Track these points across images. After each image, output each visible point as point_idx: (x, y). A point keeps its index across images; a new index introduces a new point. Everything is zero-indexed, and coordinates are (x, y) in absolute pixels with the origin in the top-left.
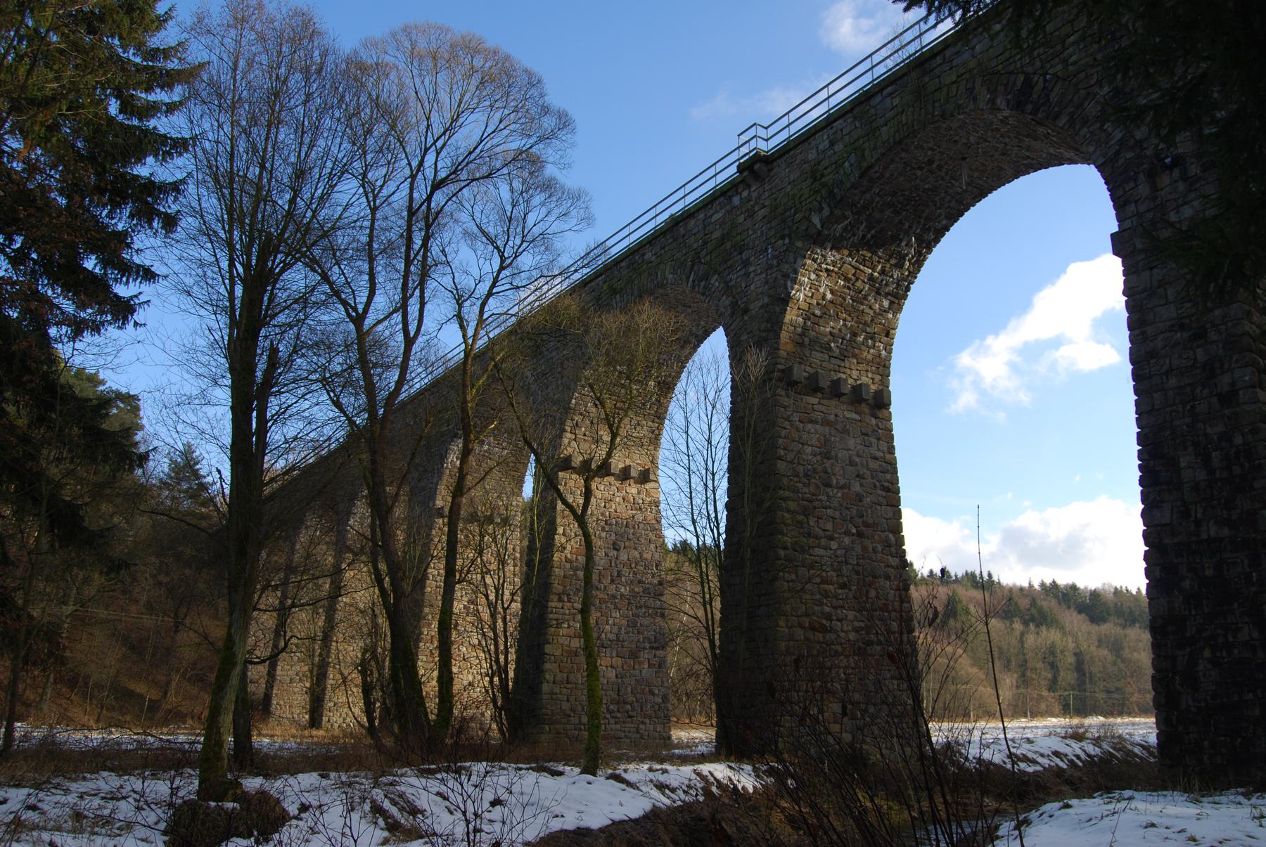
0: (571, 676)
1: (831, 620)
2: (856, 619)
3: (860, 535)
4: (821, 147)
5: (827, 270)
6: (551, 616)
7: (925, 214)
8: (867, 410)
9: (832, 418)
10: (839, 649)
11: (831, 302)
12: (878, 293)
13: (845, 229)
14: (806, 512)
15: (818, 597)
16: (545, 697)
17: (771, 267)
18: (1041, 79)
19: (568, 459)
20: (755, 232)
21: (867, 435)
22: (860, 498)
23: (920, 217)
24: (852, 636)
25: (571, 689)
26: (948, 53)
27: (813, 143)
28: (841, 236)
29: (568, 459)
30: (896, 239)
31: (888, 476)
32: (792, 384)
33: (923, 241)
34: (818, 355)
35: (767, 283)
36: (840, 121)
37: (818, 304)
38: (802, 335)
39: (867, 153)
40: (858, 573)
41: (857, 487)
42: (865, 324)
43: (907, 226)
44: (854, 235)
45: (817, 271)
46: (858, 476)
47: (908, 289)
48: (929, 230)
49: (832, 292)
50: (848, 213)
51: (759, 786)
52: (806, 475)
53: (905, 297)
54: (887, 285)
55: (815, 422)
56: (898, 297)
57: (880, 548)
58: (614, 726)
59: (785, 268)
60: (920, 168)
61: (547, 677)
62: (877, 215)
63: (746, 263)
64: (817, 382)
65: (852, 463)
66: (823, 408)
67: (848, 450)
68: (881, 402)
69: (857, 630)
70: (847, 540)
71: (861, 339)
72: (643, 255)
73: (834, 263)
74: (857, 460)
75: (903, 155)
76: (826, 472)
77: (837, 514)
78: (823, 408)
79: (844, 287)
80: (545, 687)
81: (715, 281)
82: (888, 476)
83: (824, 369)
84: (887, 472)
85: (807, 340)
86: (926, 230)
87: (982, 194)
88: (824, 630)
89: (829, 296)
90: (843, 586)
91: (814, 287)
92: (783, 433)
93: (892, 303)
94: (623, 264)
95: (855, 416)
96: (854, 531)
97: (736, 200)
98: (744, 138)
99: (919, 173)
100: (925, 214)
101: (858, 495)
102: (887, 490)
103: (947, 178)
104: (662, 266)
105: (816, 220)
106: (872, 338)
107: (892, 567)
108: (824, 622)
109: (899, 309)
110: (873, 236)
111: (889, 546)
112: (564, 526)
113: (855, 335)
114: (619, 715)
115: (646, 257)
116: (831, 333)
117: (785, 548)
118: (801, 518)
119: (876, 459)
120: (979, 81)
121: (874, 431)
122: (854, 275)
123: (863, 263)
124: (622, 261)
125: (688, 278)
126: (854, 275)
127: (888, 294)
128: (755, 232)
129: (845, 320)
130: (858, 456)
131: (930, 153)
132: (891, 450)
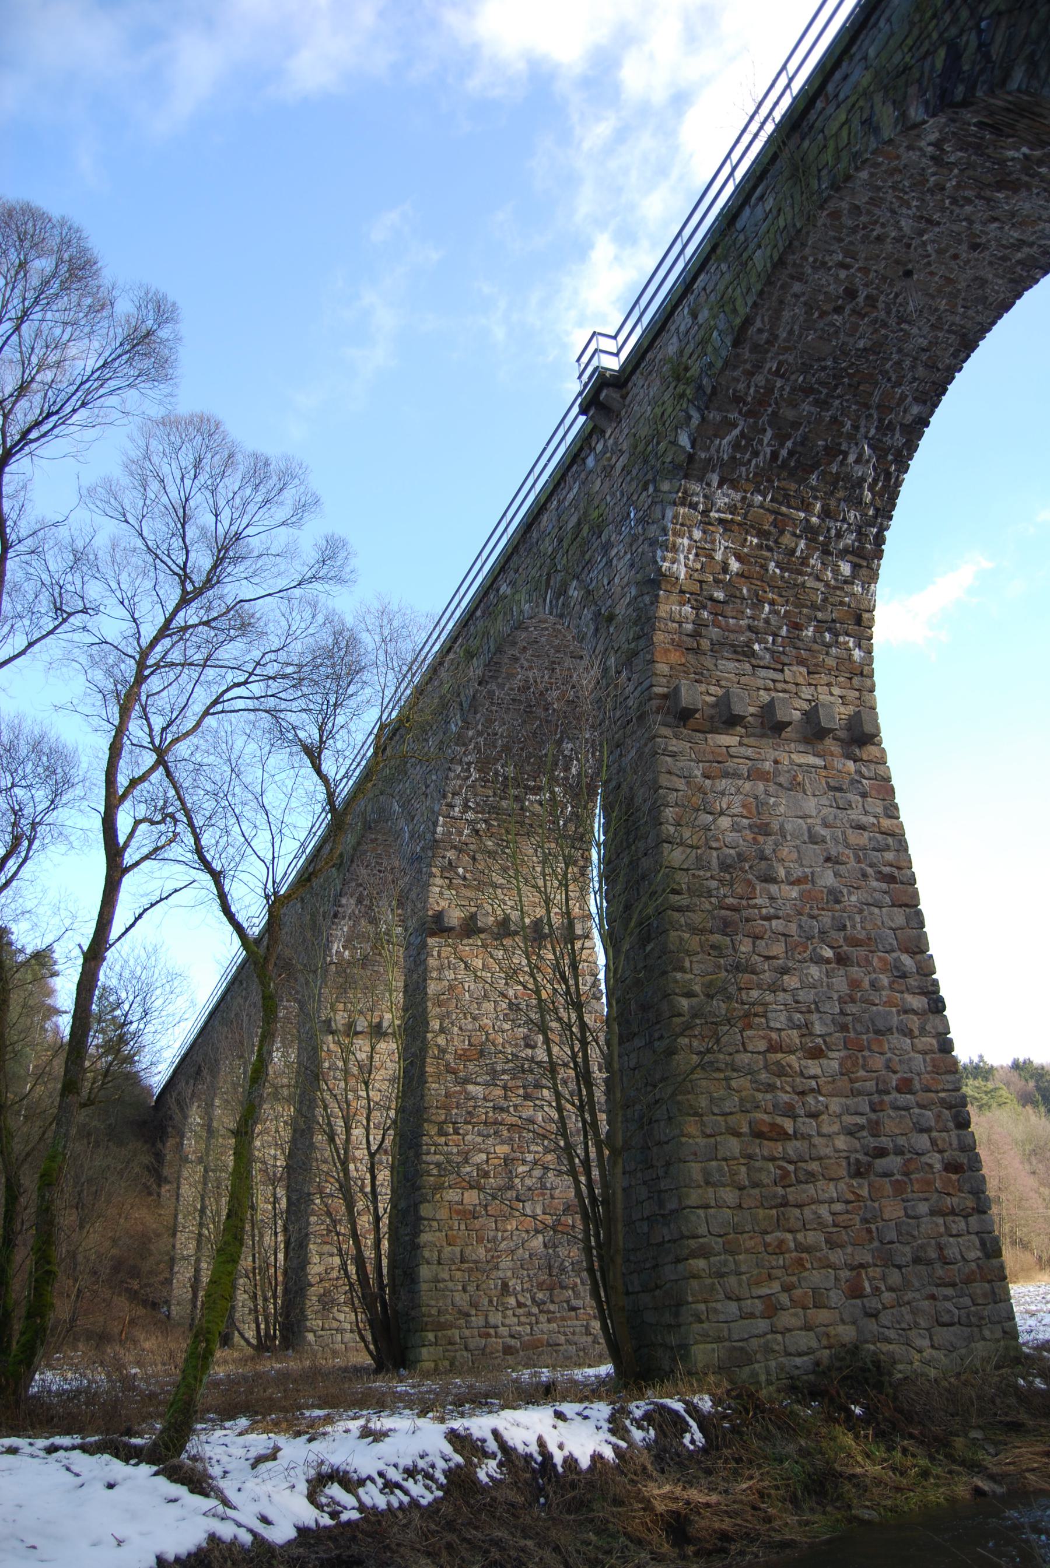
0: (468, 1250)
1: (794, 1117)
2: (847, 1111)
3: (841, 960)
4: (682, 329)
5: (721, 521)
6: (428, 1158)
7: (876, 399)
8: (836, 749)
9: (768, 766)
10: (814, 1166)
11: (740, 575)
12: (826, 552)
13: (736, 446)
14: (726, 928)
15: (763, 1076)
16: (424, 1286)
17: (635, 538)
18: (973, 35)
19: (439, 916)
20: (613, 495)
21: (839, 789)
22: (835, 897)
23: (867, 406)
24: (841, 1142)
25: (471, 1270)
26: (830, 88)
27: (673, 328)
28: (733, 458)
29: (439, 916)
30: (833, 452)
31: (889, 856)
32: (684, 716)
33: (887, 451)
34: (731, 665)
35: (632, 565)
36: (702, 277)
37: (717, 581)
38: (696, 635)
39: (739, 303)
40: (844, 1028)
41: (828, 879)
42: (814, 607)
43: (848, 424)
44: (756, 454)
45: (706, 523)
46: (828, 859)
47: (880, 540)
48: (891, 427)
49: (739, 558)
50: (733, 416)
51: (608, 1453)
52: (725, 867)
53: (879, 554)
54: (839, 535)
55: (736, 775)
56: (867, 556)
57: (885, 980)
58: (545, 1326)
59: (653, 531)
60: (838, 310)
61: (426, 1254)
62: (789, 414)
63: (607, 546)
64: (729, 706)
65: (814, 839)
66: (749, 752)
67: (805, 817)
68: (862, 735)
69: (851, 1132)
70: (815, 971)
71: (809, 632)
72: (498, 590)
73: (732, 509)
74: (823, 832)
75: (797, 287)
76: (763, 858)
77: (793, 928)
78: (749, 752)
79: (760, 546)
80: (425, 1272)
81: (575, 592)
82: (889, 856)
83: (745, 687)
84: (887, 848)
85: (705, 644)
86: (886, 428)
87: (968, 345)
88: (783, 1136)
89: (735, 565)
90: (816, 1054)
91: (704, 552)
92: (672, 797)
93: (855, 566)
94: (479, 613)
95: (812, 760)
96: (828, 953)
97: (590, 462)
98: (585, 359)
99: (838, 319)
100: (876, 399)
101: (831, 891)
102: (891, 879)
103: (892, 322)
104: (517, 597)
105: (684, 440)
106: (829, 630)
107: (914, 1012)
108: (779, 1120)
109: (873, 576)
110: (791, 453)
111: (904, 976)
112: (442, 1019)
113: (797, 627)
114: (552, 1307)
115: (501, 592)
116: (750, 628)
117: (690, 995)
118: (716, 938)
119: (861, 827)
120: (878, 98)
121: (853, 782)
122: (774, 524)
123: (786, 499)
124: (476, 608)
125: (545, 600)
126: (774, 524)
127: (844, 553)
128: (613, 495)
129: (772, 603)
130: (826, 825)
131: (843, 274)
132: (892, 811)
